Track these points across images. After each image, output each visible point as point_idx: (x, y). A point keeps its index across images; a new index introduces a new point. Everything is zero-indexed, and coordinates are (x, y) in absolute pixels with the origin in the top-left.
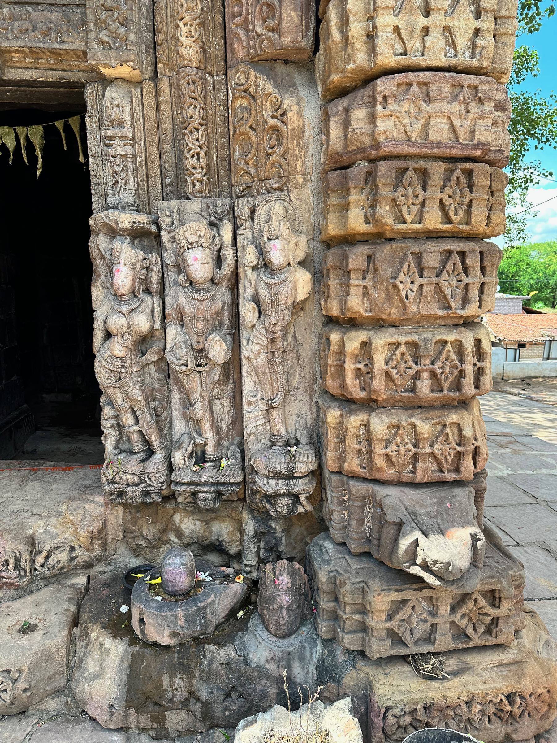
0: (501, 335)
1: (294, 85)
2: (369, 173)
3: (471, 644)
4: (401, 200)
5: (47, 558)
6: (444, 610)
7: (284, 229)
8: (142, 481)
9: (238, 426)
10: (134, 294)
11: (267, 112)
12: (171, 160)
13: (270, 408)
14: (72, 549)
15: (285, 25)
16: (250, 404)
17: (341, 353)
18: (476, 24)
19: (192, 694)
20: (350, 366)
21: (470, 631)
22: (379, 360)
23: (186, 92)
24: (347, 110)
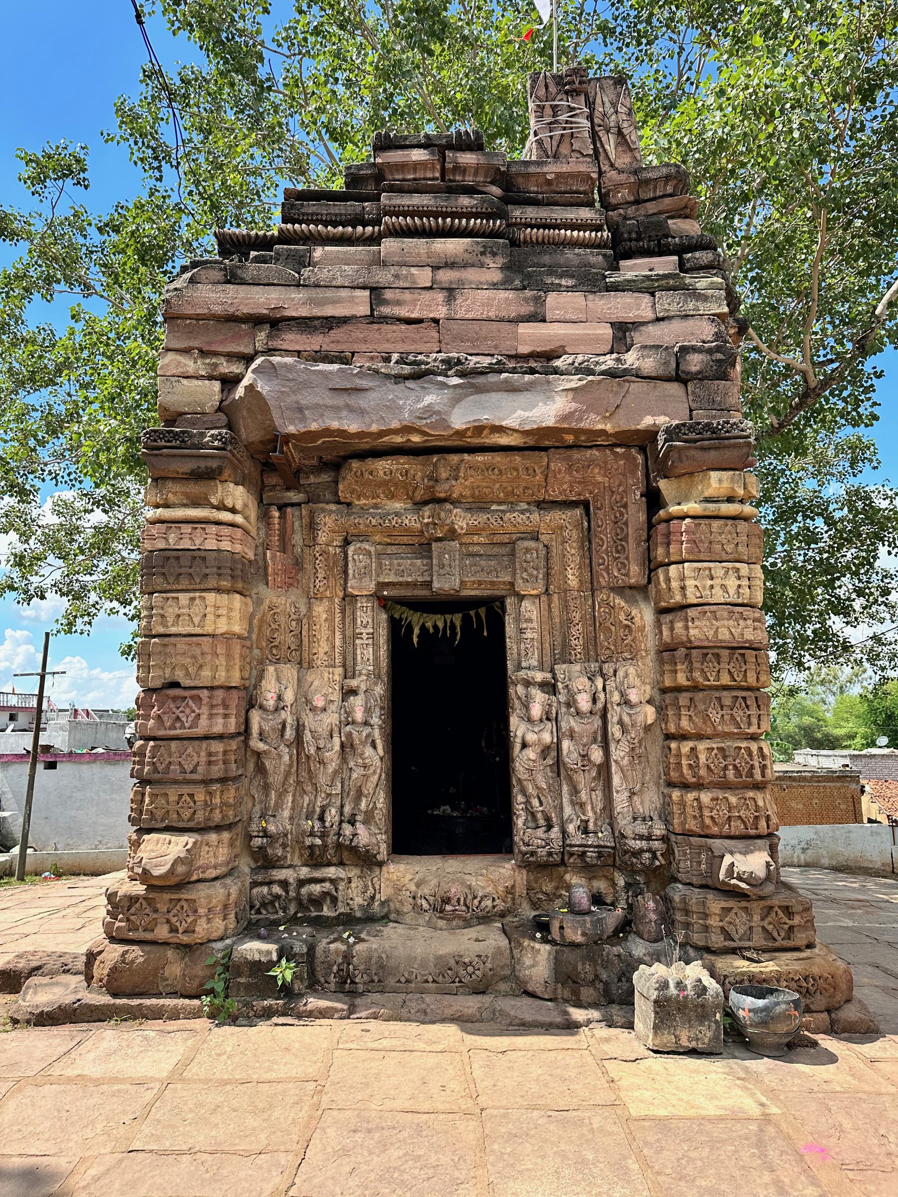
1: (637, 601)
2: (687, 655)
3: (777, 944)
4: (706, 670)
5: (480, 902)
6: (756, 918)
7: (637, 682)
8: (548, 844)
9: (607, 811)
10: (541, 721)
11: (622, 617)
12: (559, 639)
13: (633, 794)
14: (494, 899)
15: (632, 573)
16: (618, 792)
17: (679, 755)
18: (739, 582)
19: (597, 976)
20: (684, 762)
21: (775, 934)
22: (703, 758)
23: (571, 604)
24: (672, 622)
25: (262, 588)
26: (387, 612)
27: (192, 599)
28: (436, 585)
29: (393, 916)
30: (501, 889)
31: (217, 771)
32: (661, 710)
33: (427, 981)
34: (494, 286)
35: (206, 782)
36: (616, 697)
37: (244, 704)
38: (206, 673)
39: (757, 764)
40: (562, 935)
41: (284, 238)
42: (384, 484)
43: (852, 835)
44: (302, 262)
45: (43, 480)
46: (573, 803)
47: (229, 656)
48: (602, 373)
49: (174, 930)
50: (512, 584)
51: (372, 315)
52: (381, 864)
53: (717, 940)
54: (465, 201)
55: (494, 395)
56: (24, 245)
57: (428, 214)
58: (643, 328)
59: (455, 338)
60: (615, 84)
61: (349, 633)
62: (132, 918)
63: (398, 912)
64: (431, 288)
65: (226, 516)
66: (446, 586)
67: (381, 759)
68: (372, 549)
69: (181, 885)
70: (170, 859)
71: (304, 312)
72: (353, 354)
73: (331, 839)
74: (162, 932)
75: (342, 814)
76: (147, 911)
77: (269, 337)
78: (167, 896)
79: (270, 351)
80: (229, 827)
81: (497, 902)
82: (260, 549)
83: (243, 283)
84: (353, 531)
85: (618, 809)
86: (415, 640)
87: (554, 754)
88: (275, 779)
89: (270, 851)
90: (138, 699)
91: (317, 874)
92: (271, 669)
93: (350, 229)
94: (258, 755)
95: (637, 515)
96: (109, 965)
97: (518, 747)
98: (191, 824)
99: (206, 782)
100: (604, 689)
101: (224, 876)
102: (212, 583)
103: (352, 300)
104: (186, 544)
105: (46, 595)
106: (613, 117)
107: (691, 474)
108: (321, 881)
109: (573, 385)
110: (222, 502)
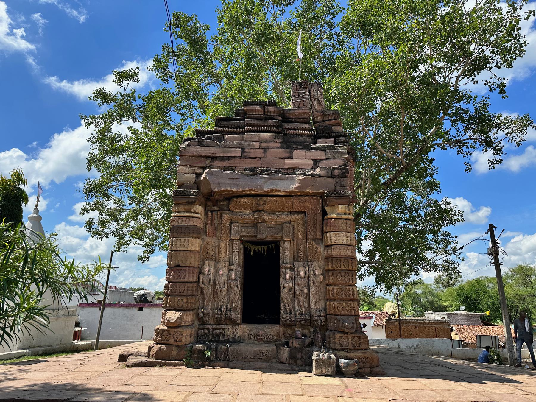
0: (467, 339)
6: (350, 340)
13: (316, 302)
17: (329, 290)
20: (330, 292)
21: (355, 345)
22: (335, 291)
24: (328, 250)
25: (205, 237)
26: (243, 245)
27: (185, 240)
28: (258, 237)
29: (242, 341)
30: (276, 333)
31: (190, 292)
32: (324, 277)
33: (251, 358)
34: (278, 148)
35: (187, 296)
36: (312, 273)
37: (198, 273)
38: (188, 262)
39: (351, 293)
40: (292, 345)
41: (216, 132)
42: (243, 205)
43: (435, 343)
44: (221, 139)
45: (116, 192)
46: (298, 306)
47: (195, 258)
48: (309, 175)
49: (175, 341)
50: (282, 237)
51: (241, 156)
52: (238, 325)
53: (338, 346)
54: (270, 122)
55: (277, 180)
56: (113, 104)
57: (259, 126)
58: (322, 161)
59: (266, 163)
60: (318, 85)
61: (231, 251)
62: (163, 336)
63: (243, 340)
64: (259, 148)
65: (196, 215)
66: (261, 237)
67: (240, 291)
68: (239, 225)
69: (178, 327)
70: (176, 318)
71: (221, 155)
72: (235, 167)
73: (223, 316)
74: (172, 341)
75: (227, 308)
76: (167, 334)
77: (210, 162)
78: (174, 330)
79: (211, 167)
80: (193, 310)
81: (274, 337)
82: (205, 225)
83: (203, 146)
84: (233, 219)
85: (312, 308)
86: (252, 254)
87: (293, 290)
88: (207, 296)
89: (204, 319)
90: (167, 270)
91: (219, 327)
92: (207, 262)
93: (236, 130)
94: (202, 288)
95: (319, 217)
96: (156, 350)
97: (282, 287)
98: (181, 308)
99: (187, 296)
100: (309, 270)
101: (191, 325)
102: (191, 235)
103: (236, 152)
104: (184, 223)
105: (109, 236)
106: (317, 95)
107: (334, 206)
108: (220, 329)
109: (300, 178)
110: (195, 211)
